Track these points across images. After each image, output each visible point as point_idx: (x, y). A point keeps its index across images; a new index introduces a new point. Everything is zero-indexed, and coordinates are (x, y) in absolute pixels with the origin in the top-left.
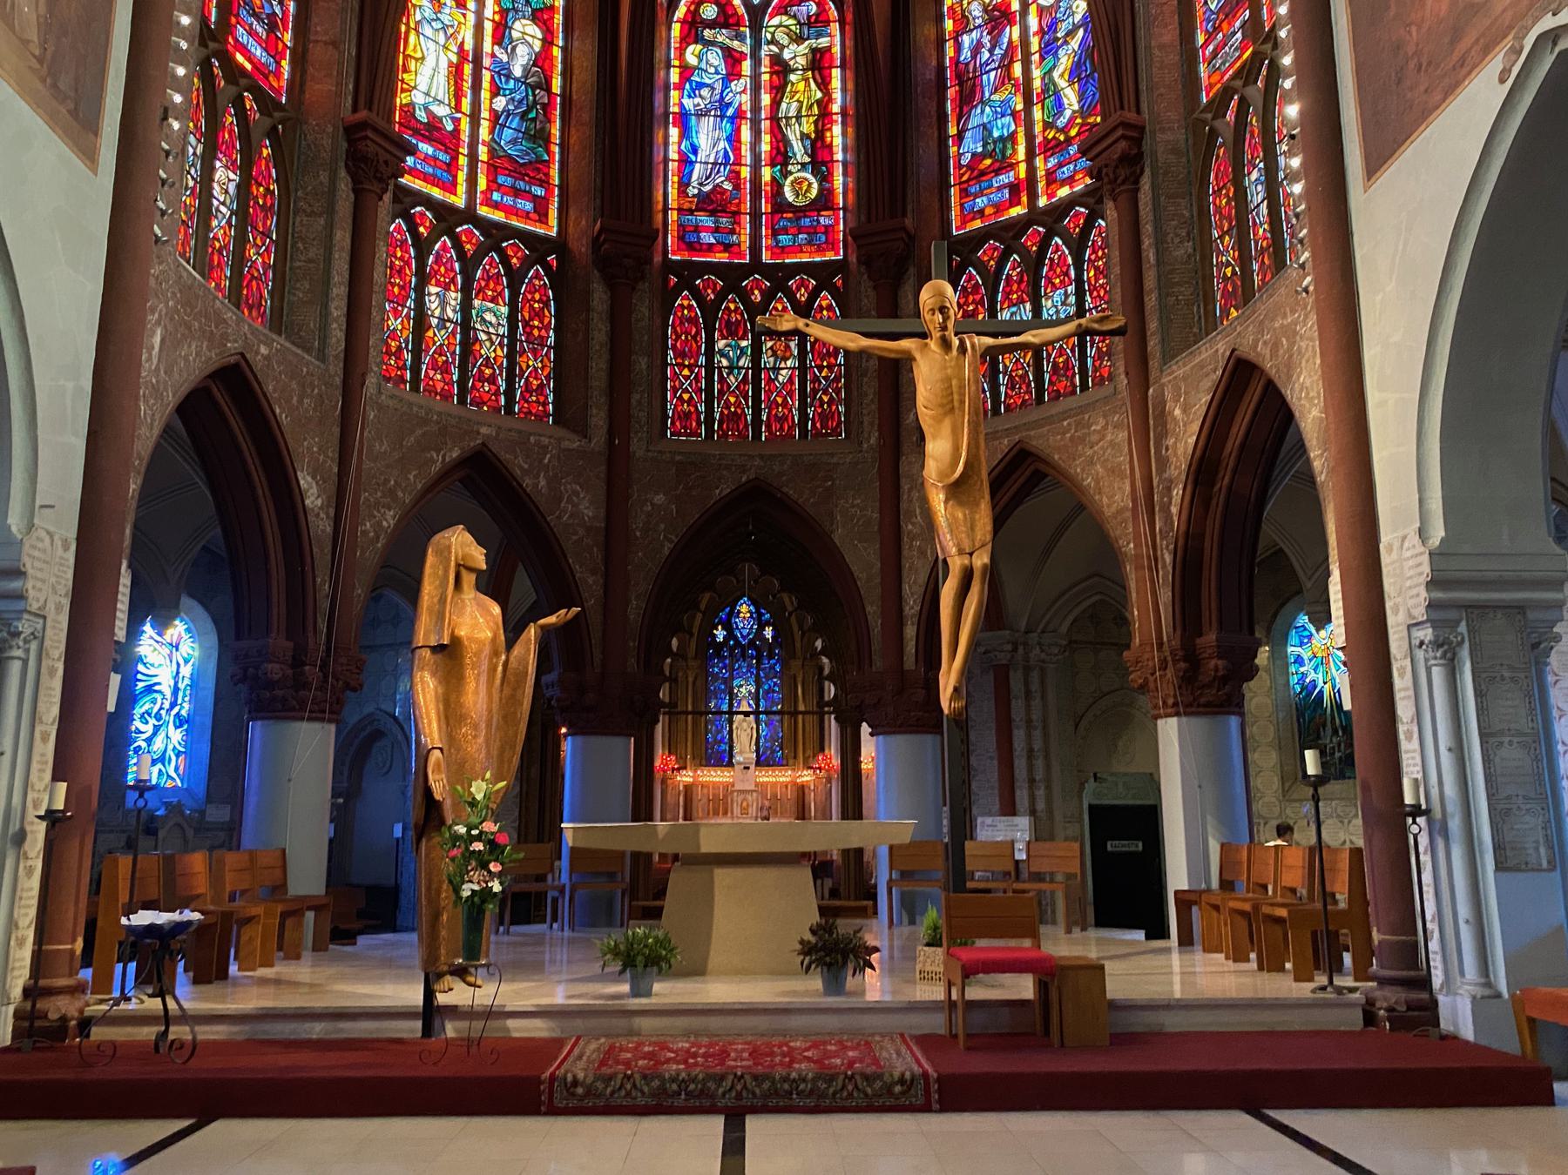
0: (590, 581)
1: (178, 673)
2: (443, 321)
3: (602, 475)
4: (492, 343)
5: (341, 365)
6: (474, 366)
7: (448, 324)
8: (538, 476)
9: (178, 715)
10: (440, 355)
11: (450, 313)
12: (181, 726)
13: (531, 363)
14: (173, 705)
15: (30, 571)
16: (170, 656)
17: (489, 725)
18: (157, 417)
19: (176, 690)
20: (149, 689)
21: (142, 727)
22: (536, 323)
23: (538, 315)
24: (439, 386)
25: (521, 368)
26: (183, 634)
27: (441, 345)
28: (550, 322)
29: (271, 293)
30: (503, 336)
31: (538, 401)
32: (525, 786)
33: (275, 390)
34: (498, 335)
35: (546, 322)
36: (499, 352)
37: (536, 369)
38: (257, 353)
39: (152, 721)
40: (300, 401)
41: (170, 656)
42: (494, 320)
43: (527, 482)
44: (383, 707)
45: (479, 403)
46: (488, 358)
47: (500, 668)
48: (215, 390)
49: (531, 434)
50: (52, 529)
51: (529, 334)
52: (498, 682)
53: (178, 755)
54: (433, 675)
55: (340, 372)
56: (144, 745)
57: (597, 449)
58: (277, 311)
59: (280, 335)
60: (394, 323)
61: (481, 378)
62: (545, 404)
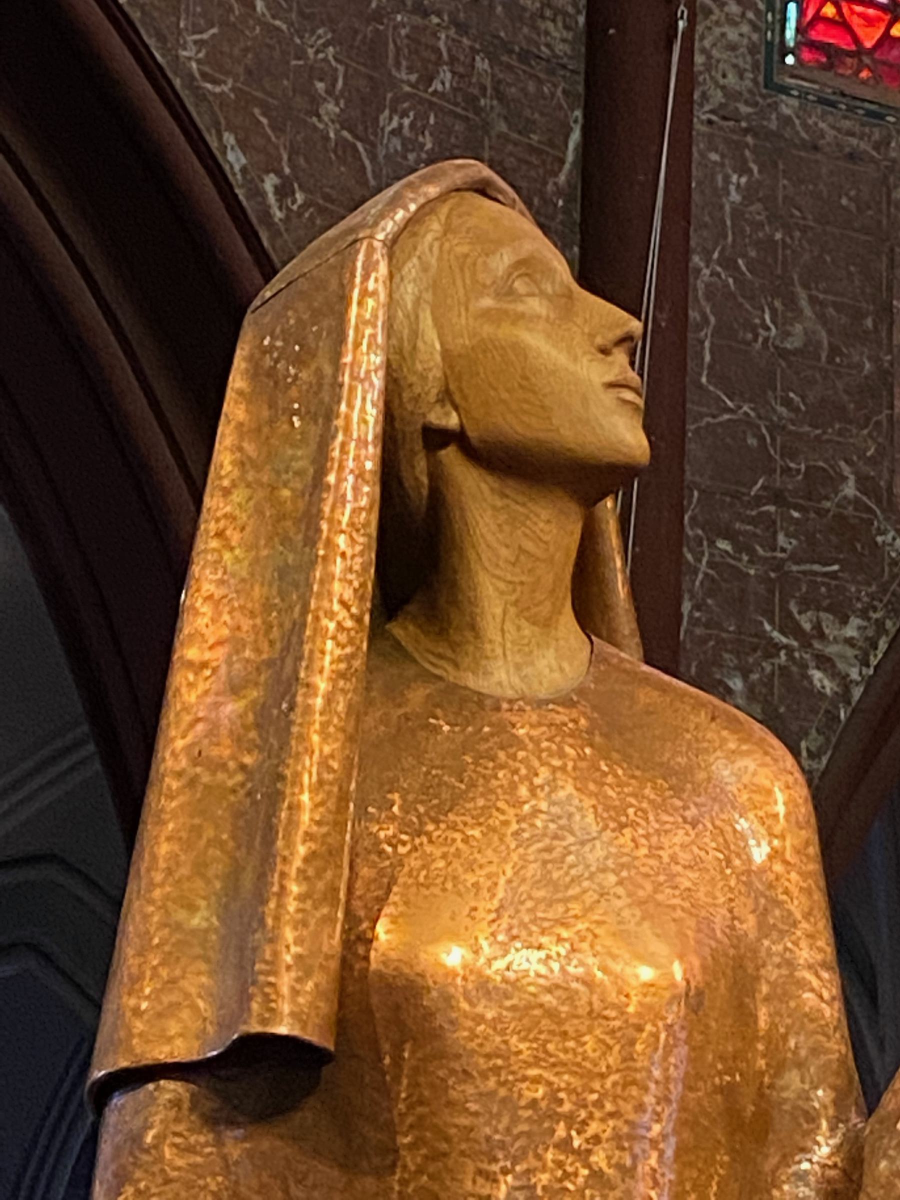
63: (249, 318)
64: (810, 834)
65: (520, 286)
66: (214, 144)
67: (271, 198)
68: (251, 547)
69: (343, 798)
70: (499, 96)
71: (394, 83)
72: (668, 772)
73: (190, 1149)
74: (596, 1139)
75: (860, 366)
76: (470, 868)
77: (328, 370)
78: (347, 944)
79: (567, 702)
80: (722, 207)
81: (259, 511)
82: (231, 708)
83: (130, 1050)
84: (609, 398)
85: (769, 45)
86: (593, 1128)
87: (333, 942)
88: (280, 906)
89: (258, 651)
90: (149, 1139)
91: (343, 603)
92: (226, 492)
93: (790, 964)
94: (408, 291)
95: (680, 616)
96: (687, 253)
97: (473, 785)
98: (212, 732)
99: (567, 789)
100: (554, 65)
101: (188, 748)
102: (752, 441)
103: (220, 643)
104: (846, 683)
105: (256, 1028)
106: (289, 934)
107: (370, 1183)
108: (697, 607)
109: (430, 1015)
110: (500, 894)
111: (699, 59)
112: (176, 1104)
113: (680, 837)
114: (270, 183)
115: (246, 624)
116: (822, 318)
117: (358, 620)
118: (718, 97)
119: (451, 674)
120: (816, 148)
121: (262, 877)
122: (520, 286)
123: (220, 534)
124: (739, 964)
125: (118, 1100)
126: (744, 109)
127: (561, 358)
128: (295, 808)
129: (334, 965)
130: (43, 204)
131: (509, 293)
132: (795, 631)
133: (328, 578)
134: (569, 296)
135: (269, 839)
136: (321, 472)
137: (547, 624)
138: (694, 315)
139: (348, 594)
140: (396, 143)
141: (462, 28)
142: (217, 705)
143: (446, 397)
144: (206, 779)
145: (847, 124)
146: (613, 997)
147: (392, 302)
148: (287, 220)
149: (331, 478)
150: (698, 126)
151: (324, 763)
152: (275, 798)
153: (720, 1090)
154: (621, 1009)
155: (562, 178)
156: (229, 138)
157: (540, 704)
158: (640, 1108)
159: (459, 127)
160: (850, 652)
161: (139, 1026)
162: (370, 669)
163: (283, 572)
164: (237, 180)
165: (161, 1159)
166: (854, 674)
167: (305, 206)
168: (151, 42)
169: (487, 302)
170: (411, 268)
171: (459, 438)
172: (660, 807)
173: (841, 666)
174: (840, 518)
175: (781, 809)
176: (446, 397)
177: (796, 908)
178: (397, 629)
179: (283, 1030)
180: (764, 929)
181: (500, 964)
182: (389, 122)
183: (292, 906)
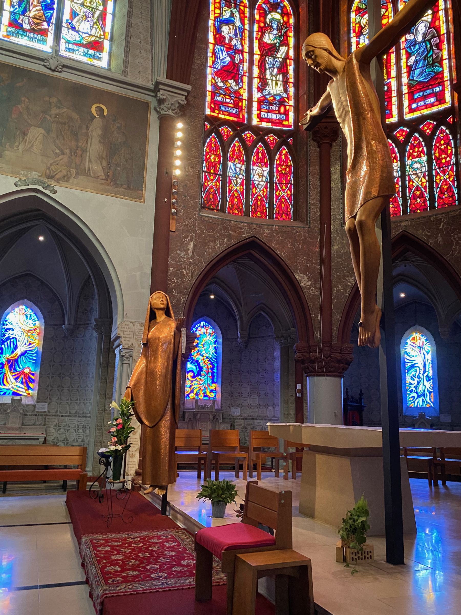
1: (425, 358)
4: (419, 178)
8: (436, 237)
9: (427, 376)
12: (430, 380)
13: (442, 178)
14: (424, 372)
15: (122, 335)
16: (420, 352)
19: (425, 365)
20: (413, 366)
21: (412, 382)
23: (444, 151)
26: (424, 341)
36: (424, 180)
39: (416, 379)
41: (420, 352)
46: (418, 186)
50: (133, 321)
53: (430, 393)
56: (414, 389)
62: (453, 195)
100: (316, 232)
114: (283, 253)
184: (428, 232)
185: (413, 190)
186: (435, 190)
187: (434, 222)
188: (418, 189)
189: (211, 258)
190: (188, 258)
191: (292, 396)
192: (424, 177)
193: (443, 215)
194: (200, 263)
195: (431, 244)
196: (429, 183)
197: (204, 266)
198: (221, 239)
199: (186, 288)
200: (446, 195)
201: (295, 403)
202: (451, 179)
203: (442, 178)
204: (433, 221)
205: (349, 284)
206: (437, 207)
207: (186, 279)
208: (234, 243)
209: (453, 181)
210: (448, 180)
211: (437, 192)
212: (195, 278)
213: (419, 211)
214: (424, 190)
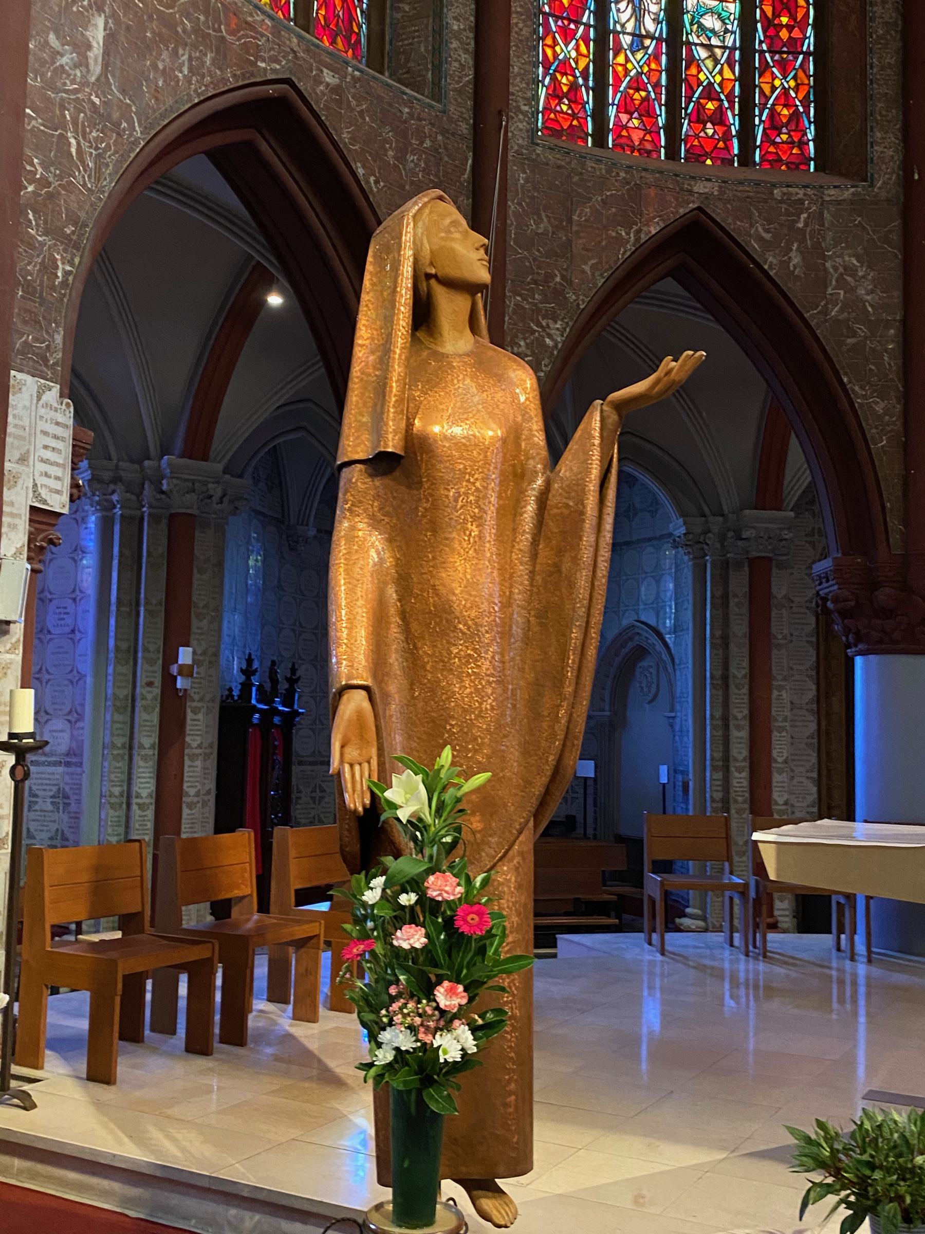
0: (879, 408)
2: (639, 37)
3: (894, 237)
4: (716, 62)
5: (470, 103)
6: (689, 99)
7: (647, 42)
10: (637, 90)
11: (650, 25)
13: (777, 83)
17: (505, 633)
18: (111, 158)
22: (784, 20)
24: (636, 136)
25: (761, 92)
27: (640, 74)
28: (807, 14)
29: (367, 14)
30: (733, 49)
31: (791, 143)
32: (824, 723)
33: (354, 140)
34: (724, 48)
35: (800, 16)
36: (728, 74)
37: (785, 91)
38: (318, 81)
40: (401, 157)
42: (718, 25)
43: (771, 262)
44: (643, 619)
45: (696, 156)
46: (710, 84)
47: (530, 508)
48: (264, 146)
49: (774, 186)
51: (772, 39)
52: (525, 539)
54: (375, 524)
55: (469, 115)
57: (884, 195)
58: (377, 38)
59: (382, 73)
60: (567, 51)
61: (699, 118)
62: (803, 144)
63: (373, 239)
64: (537, 393)
65: (452, 229)
66: (354, 167)
67: (373, 185)
68: (376, 310)
69: (405, 384)
70: (446, 149)
71: (411, 144)
72: (496, 375)
73: (365, 483)
74: (477, 479)
75: (561, 238)
76: (441, 404)
77: (396, 255)
78: (407, 426)
79: (468, 355)
80: (517, 185)
81: (377, 299)
82: (372, 358)
83: (347, 456)
84: (479, 263)
85: (532, 129)
86: (476, 476)
87: (403, 425)
88: (388, 415)
89: (378, 340)
90: (354, 480)
91: (404, 327)
92: (368, 293)
93: (531, 430)
94: (420, 231)
95: (504, 322)
96: (506, 200)
97: (441, 380)
98: (367, 365)
99: (468, 381)
100: (462, 137)
101: (360, 370)
102: (527, 264)
103: (367, 339)
104: (556, 343)
105: (382, 450)
106: (391, 423)
107: (415, 492)
108: (510, 319)
109: (430, 445)
110: (450, 411)
111: (510, 134)
112: (361, 470)
113: (500, 394)
114: (372, 179)
115: (375, 332)
116: (549, 221)
117: (407, 331)
118: (516, 148)
119: (433, 346)
120: (547, 164)
121: (383, 406)
122: (452, 229)
123: (367, 306)
124: (516, 431)
125: (344, 470)
126: (524, 151)
127: (464, 252)
128: (391, 387)
129: (404, 432)
130: (283, 163)
131: (448, 231)
132: (541, 326)
133: (399, 319)
134: (467, 232)
135: (384, 396)
136: (396, 287)
137: (461, 332)
138: (509, 222)
139: (404, 324)
140: (412, 165)
141: (433, 125)
142: (368, 357)
143: (431, 264)
144: (365, 378)
145: (558, 156)
146: (481, 440)
147: (415, 235)
148: (378, 192)
149: (398, 289)
150: (510, 158)
151: (399, 375)
152: (385, 384)
153: (511, 465)
154: (483, 443)
155: (466, 176)
156: (359, 165)
157: (461, 355)
158: (489, 470)
159: (432, 159)
160: (558, 333)
161: (350, 449)
162: (411, 345)
163: (385, 317)
164: (361, 178)
165: (357, 486)
166: (559, 339)
167: (384, 187)
168: (333, 132)
169: (443, 235)
170: (420, 224)
171: (435, 276)
172: (494, 385)
173: (555, 337)
174: (555, 288)
175: (529, 386)
176: (431, 264)
177: (533, 414)
178: (418, 334)
179: (390, 450)
180: (524, 420)
181: (450, 431)
182: (410, 158)
183: (391, 415)
184: (767, 231)
185: (696, 95)
186: (757, 113)
187: (784, 206)
188: (710, 93)
189: (163, 116)
190: (84, 83)
191: (150, 684)
192: (730, 62)
193: (809, 191)
194: (124, 125)
195: (770, 267)
196: (740, 86)
197: (137, 141)
198: (196, 48)
199: (74, 220)
200: (784, 137)
201: (157, 710)
202: (801, 96)
203: (777, 83)
204: (781, 202)
205: (548, 341)
206: (760, 164)
207: (79, 178)
208: (232, 83)
209: (805, 103)
210: (793, 94)
211: (760, 120)
212: (108, 184)
213: (709, 162)
214: (726, 104)
